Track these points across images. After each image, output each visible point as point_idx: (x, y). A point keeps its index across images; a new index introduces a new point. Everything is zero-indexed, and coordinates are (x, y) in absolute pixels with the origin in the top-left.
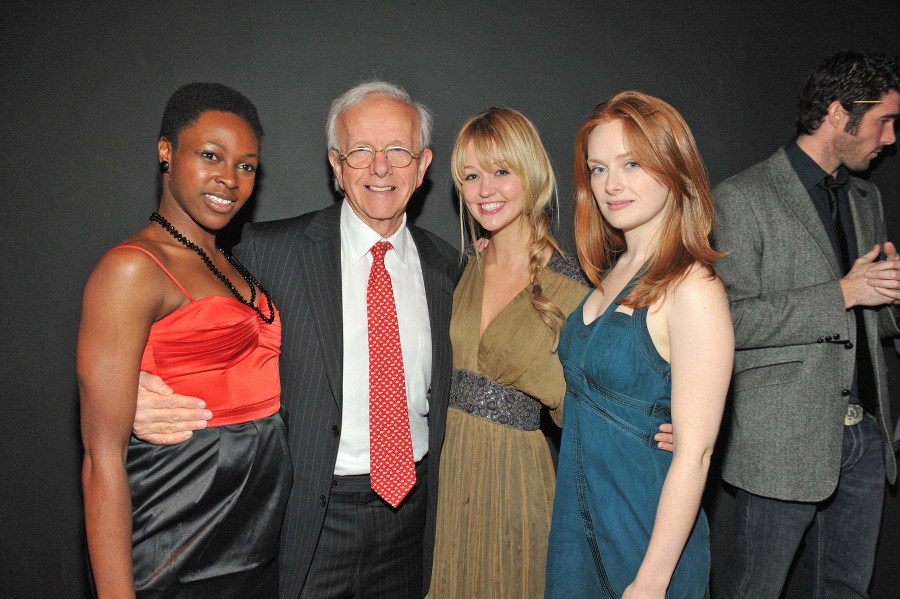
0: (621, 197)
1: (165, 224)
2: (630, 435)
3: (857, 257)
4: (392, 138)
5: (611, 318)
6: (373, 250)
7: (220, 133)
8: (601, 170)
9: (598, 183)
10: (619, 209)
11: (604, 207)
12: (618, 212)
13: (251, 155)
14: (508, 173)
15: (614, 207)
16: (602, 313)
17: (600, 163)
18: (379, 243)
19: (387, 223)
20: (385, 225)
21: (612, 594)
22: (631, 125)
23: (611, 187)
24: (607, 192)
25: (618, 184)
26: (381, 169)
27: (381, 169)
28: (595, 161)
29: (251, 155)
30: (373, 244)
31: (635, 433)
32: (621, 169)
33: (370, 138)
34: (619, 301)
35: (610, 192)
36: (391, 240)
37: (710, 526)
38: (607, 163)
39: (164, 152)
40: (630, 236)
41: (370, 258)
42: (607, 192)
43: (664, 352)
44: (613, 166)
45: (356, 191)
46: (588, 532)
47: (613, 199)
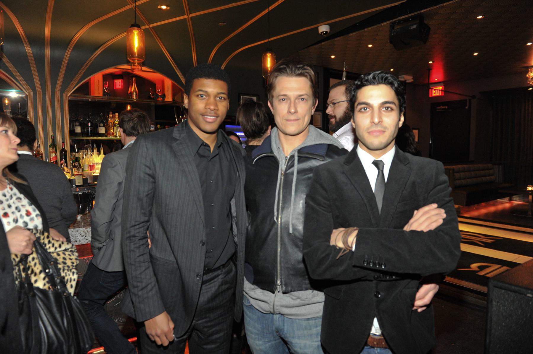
13: (223, 93)
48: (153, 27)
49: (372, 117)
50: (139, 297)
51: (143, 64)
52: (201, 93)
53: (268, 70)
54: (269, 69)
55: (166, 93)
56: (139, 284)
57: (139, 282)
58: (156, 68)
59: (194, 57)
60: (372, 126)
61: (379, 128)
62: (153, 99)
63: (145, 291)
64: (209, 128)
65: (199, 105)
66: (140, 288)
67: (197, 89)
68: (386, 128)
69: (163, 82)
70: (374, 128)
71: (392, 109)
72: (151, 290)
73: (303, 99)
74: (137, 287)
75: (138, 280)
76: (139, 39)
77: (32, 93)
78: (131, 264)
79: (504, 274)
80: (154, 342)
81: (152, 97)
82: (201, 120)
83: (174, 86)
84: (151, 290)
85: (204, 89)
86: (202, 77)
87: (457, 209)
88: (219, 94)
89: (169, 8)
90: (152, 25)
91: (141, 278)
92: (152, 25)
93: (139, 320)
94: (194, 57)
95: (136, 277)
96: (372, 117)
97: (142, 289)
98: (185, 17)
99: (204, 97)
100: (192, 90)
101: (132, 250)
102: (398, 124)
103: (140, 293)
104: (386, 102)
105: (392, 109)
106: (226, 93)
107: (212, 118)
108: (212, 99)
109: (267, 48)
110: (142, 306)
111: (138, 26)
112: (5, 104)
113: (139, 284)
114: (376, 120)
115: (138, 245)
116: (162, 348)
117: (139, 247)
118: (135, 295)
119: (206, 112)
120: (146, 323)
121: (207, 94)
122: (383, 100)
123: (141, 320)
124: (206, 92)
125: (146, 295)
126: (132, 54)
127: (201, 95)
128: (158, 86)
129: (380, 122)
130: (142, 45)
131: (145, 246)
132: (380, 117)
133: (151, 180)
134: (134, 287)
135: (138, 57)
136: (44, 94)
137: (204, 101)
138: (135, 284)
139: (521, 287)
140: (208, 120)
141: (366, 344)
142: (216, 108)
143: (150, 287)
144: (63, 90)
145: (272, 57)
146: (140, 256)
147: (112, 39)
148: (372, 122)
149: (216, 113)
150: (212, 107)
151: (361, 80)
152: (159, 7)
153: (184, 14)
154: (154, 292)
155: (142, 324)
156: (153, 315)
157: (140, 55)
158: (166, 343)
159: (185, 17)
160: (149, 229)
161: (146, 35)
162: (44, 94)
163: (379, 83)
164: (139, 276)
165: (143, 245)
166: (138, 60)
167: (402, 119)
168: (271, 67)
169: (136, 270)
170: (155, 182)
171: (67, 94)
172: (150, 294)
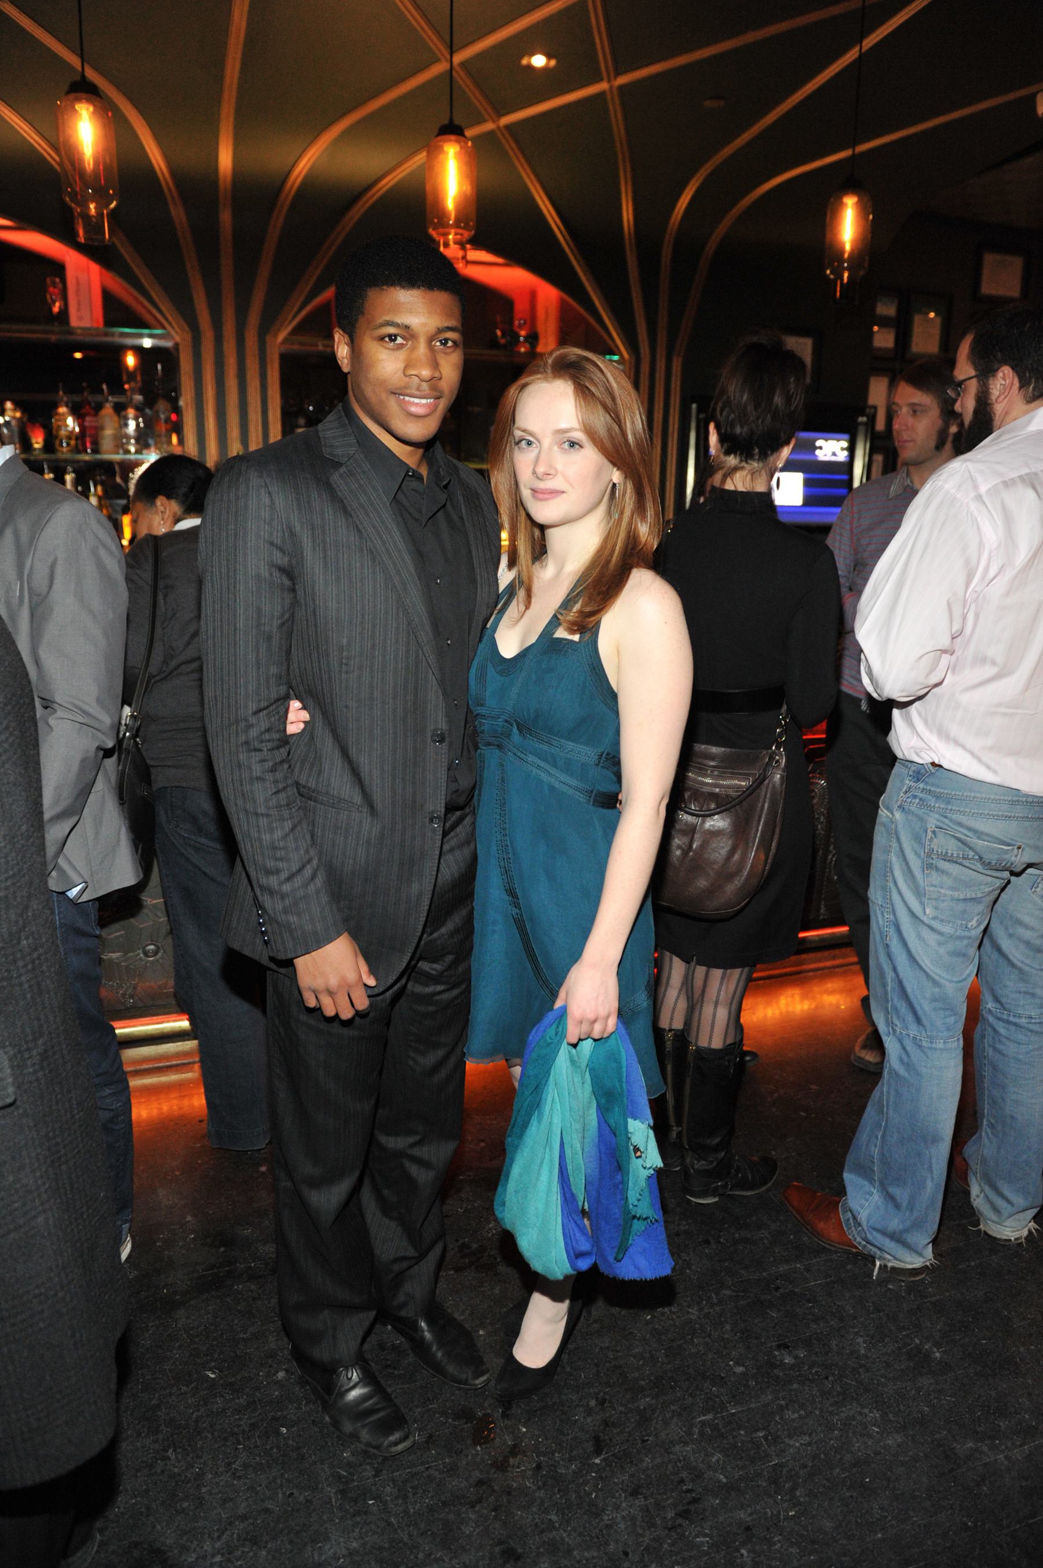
2: (565, 789)
5: (547, 645)
8: (529, 443)
9: (524, 461)
10: (545, 500)
11: (526, 493)
12: (544, 503)
13: (449, 329)
14: (581, 447)
15: (541, 496)
16: (532, 640)
17: (531, 434)
21: (546, 983)
23: (541, 470)
24: (534, 472)
25: (551, 467)
28: (524, 431)
29: (449, 329)
31: (576, 789)
32: (556, 448)
34: (555, 622)
35: (540, 476)
37: (873, 1025)
38: (539, 436)
40: (554, 537)
42: (534, 472)
43: (615, 689)
44: (547, 442)
46: (515, 911)
47: (542, 485)
48: (508, 127)
50: (283, 897)
51: (477, 242)
52: (392, 330)
53: (843, 251)
54: (848, 247)
55: (540, 329)
56: (280, 865)
57: (281, 859)
58: (512, 251)
59: (627, 214)
62: (505, 346)
63: (297, 881)
64: (418, 431)
65: (387, 364)
66: (284, 876)
67: (381, 321)
69: (533, 295)
72: (313, 878)
74: (277, 872)
75: (279, 854)
76: (460, 169)
77: (188, 337)
78: (257, 814)
79: (433, 908)
80: (318, 1010)
81: (503, 341)
82: (392, 409)
83: (564, 310)
84: (313, 878)
85: (399, 320)
86: (393, 284)
88: (440, 331)
89: (553, 63)
90: (505, 120)
91: (285, 848)
92: (505, 120)
94: (627, 214)
95: (275, 848)
97: (289, 879)
98: (603, 86)
99: (399, 340)
100: (362, 320)
101: (258, 778)
103: (286, 888)
106: (459, 326)
107: (424, 401)
108: (422, 348)
109: (846, 179)
110: (293, 919)
111: (452, 130)
112: (127, 367)
113: (280, 865)
115: (271, 764)
116: (336, 1024)
117: (273, 770)
118: (271, 892)
119: (406, 387)
121: (409, 334)
124: (407, 327)
125: (301, 893)
126: (441, 214)
127: (390, 336)
128: (521, 307)
130: (468, 188)
131: (286, 766)
133: (287, 582)
134: (269, 872)
135: (457, 224)
136: (219, 339)
137: (402, 355)
138: (270, 864)
140: (413, 409)
142: (437, 375)
143: (308, 872)
144: (265, 328)
145: (863, 210)
146: (278, 792)
147: (400, 164)
149: (434, 388)
150: (426, 373)
152: (524, 62)
153: (598, 79)
154: (319, 881)
155: (289, 963)
156: (318, 942)
157: (461, 220)
158: (347, 1014)
159: (603, 86)
160: (140, 734)
161: (482, 155)
162: (219, 339)
164: (282, 844)
165: (282, 762)
166: (456, 234)
168: (854, 242)
169: (271, 830)
170: (293, 590)
171: (276, 335)
172: (312, 888)
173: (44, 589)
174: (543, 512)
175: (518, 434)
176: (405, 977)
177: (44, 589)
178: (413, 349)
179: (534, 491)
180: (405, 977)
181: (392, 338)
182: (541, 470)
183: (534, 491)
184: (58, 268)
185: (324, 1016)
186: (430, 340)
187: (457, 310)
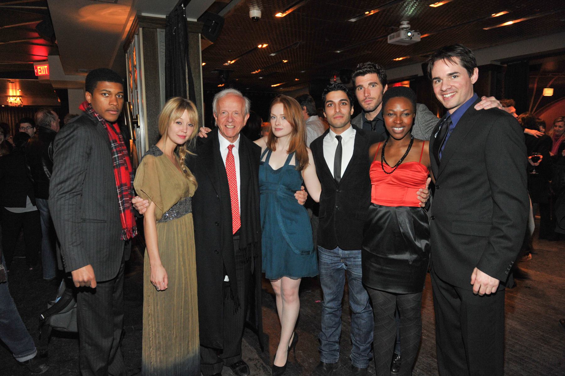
0: (279, 127)
1: (410, 146)
3: (371, 164)
4: (234, 110)
5: (376, 119)
6: (228, 147)
7: (111, 87)
9: (273, 121)
11: (273, 129)
18: (230, 145)
19: (232, 138)
20: (232, 139)
22: (285, 107)
23: (277, 124)
26: (230, 120)
27: (230, 120)
30: (228, 145)
33: (227, 109)
36: (234, 144)
39: (88, 97)
41: (227, 151)
44: (279, 117)
45: (222, 127)
47: (277, 127)
49: (335, 109)
52: (105, 92)
60: (335, 114)
61: (340, 115)
68: (343, 114)
70: (337, 115)
71: (346, 104)
73: (343, 103)
87: (531, 159)
88: (119, 93)
93: (67, 271)
96: (335, 109)
99: (107, 95)
102: (350, 113)
104: (342, 100)
105: (346, 104)
108: (114, 97)
114: (338, 111)
120: (72, 272)
122: (339, 100)
123: (69, 271)
129: (340, 111)
132: (340, 109)
139: (63, 262)
141: (547, 231)
148: (336, 112)
151: (327, 88)
155: (70, 274)
163: (337, 90)
167: (353, 110)
173: (62, 269)
174: (278, 134)
175: (272, 115)
176: (111, 356)
177: (62, 269)
178: (111, 97)
179: (276, 129)
180: (111, 356)
181: (105, 94)
182: (277, 124)
183: (276, 129)
184: (422, 34)
185: (474, 294)
186: (116, 95)
187: (122, 88)
